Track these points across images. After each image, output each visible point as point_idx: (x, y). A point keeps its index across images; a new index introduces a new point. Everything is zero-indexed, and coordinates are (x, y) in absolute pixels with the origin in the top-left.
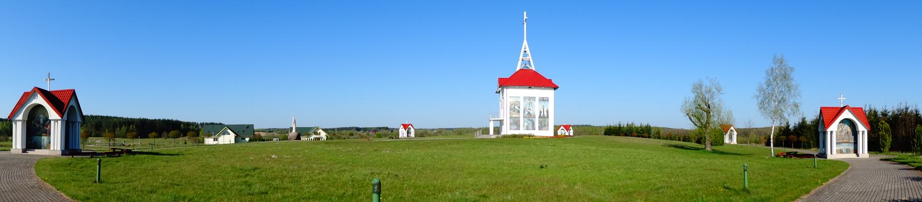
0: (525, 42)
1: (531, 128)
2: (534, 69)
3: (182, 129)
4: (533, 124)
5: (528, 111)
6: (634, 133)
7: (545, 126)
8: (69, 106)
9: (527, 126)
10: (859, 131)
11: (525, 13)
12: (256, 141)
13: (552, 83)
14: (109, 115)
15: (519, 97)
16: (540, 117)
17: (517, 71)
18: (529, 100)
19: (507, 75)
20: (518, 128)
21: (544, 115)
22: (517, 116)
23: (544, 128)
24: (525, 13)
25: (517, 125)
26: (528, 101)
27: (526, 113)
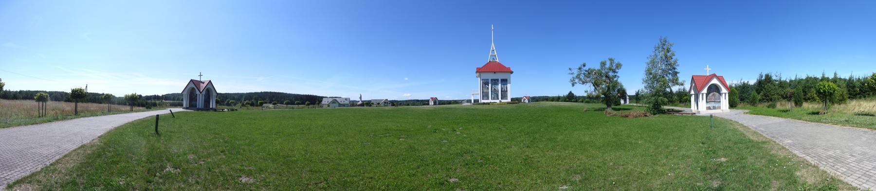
1: (496, 98)
4: (498, 96)
16: (502, 91)
20: (488, 99)
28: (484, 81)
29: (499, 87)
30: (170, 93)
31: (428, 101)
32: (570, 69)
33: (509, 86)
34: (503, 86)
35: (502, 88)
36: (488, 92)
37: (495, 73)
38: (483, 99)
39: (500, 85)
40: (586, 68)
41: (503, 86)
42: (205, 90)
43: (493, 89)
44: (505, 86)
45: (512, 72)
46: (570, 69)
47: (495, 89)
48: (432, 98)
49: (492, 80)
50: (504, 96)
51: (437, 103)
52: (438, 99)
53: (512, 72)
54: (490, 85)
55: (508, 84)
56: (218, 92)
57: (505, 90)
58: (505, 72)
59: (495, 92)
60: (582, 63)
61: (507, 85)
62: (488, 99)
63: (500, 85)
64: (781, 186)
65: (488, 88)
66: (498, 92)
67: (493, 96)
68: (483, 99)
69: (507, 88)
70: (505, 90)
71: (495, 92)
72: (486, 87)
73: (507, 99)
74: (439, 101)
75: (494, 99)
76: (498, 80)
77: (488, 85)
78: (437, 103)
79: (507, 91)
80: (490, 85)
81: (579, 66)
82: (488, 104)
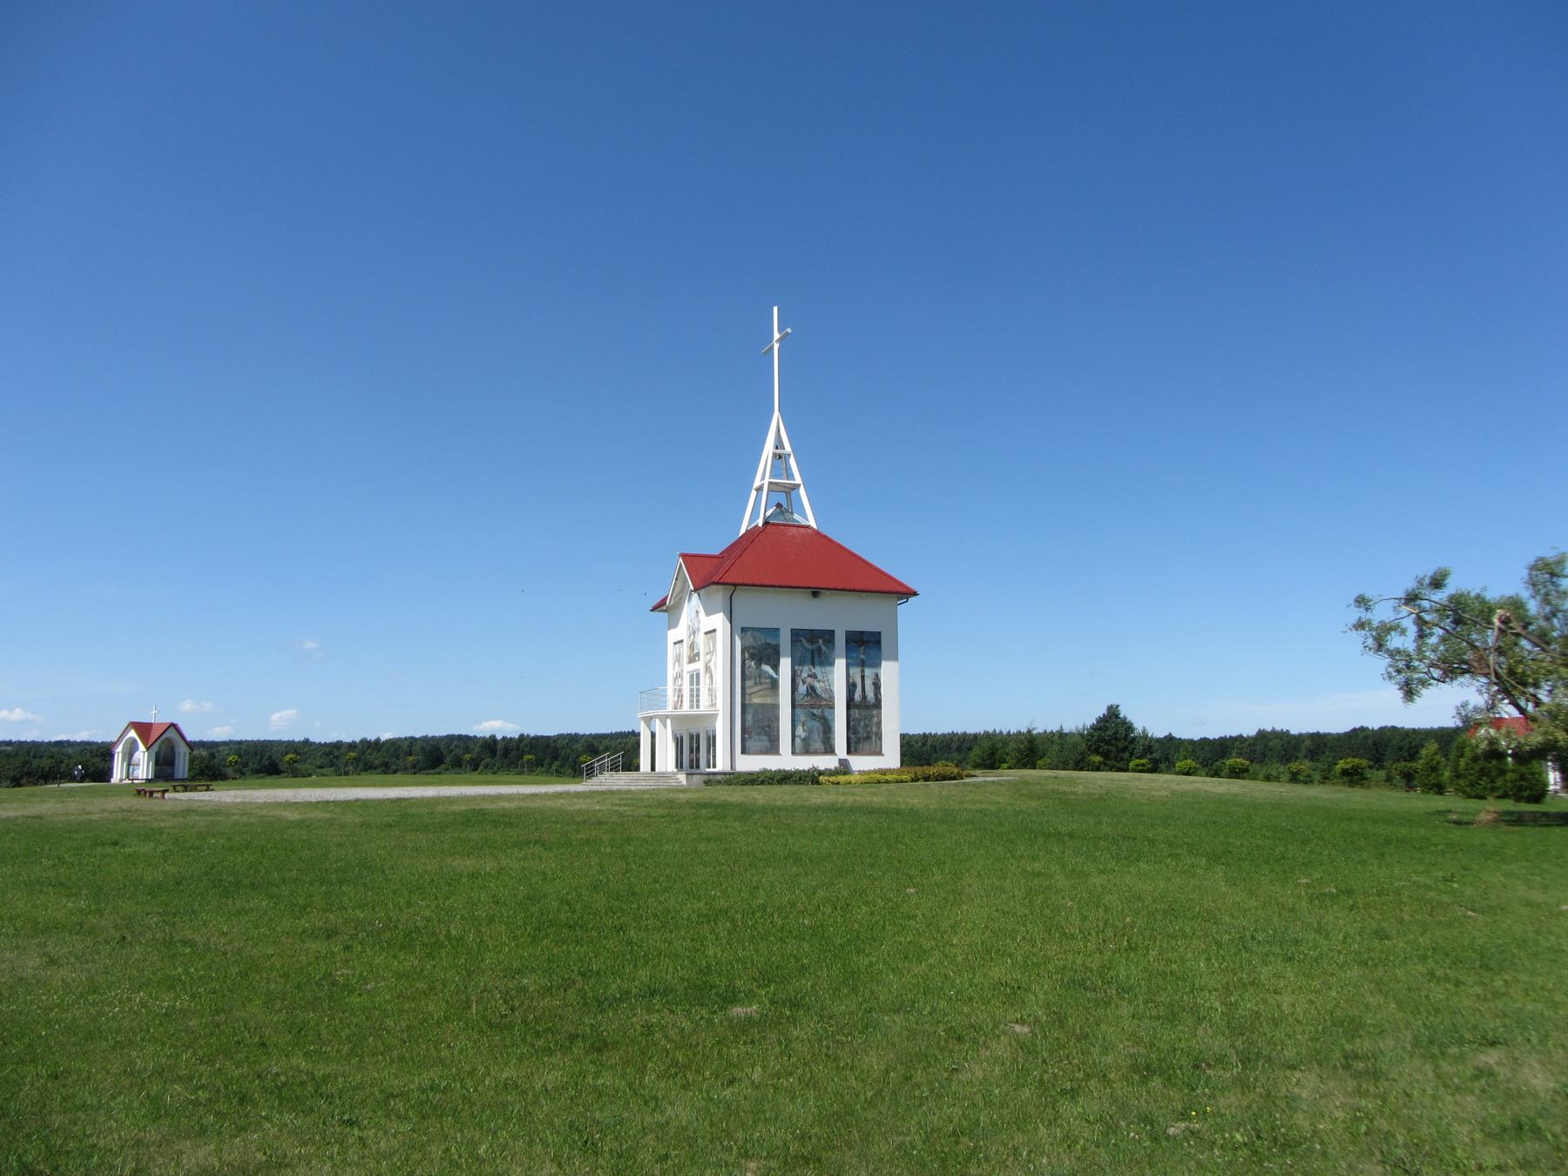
0: (776, 413)
1: (819, 745)
2: (812, 523)
3: (1461, 725)
4: (828, 730)
5: (809, 680)
6: (564, 795)
7: (868, 738)
8: (163, 737)
9: (804, 740)
10: (179, 754)
11: (775, 309)
12: (182, 811)
13: (721, 557)
14: (959, 728)
15: (714, 631)
16: (850, 703)
17: (740, 535)
18: (811, 641)
19: (714, 544)
20: (773, 748)
21: (864, 696)
22: (769, 701)
23: (866, 746)
24: (775, 309)
25: (767, 734)
26: (807, 645)
27: (802, 689)
28: (750, 641)
29: (838, 675)
30: (403, 736)
31: (104, 753)
32: (1362, 601)
33: (888, 671)
34: (856, 672)
35: (851, 688)
36: (775, 707)
37: (815, 594)
38: (744, 751)
39: (840, 664)
40: (1452, 587)
41: (856, 672)
42: (159, 742)
43: (802, 689)
44: (868, 672)
45: (907, 593)
46: (1362, 601)
47: (812, 689)
48: (143, 729)
49: (796, 634)
50: (863, 736)
51: (182, 767)
52: (190, 737)
53: (907, 593)
54: (785, 664)
55: (884, 663)
56: (189, 738)
57: (870, 695)
58: (854, 591)
59: (812, 706)
60: (1428, 571)
61: (878, 665)
62: (773, 748)
63: (840, 664)
64: (420, 898)
65: (774, 684)
66: (832, 707)
67: (800, 731)
68: (744, 751)
69: (877, 686)
70: (870, 695)
71: (812, 706)
72: (761, 674)
73: (879, 753)
74: (192, 746)
75: (807, 751)
76: (829, 636)
77: (776, 667)
78: (182, 767)
79: (877, 704)
80: (785, 664)
81: (1411, 584)
82: (784, 778)
